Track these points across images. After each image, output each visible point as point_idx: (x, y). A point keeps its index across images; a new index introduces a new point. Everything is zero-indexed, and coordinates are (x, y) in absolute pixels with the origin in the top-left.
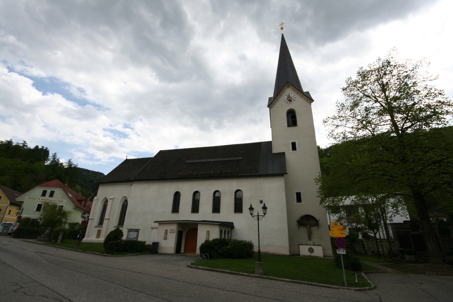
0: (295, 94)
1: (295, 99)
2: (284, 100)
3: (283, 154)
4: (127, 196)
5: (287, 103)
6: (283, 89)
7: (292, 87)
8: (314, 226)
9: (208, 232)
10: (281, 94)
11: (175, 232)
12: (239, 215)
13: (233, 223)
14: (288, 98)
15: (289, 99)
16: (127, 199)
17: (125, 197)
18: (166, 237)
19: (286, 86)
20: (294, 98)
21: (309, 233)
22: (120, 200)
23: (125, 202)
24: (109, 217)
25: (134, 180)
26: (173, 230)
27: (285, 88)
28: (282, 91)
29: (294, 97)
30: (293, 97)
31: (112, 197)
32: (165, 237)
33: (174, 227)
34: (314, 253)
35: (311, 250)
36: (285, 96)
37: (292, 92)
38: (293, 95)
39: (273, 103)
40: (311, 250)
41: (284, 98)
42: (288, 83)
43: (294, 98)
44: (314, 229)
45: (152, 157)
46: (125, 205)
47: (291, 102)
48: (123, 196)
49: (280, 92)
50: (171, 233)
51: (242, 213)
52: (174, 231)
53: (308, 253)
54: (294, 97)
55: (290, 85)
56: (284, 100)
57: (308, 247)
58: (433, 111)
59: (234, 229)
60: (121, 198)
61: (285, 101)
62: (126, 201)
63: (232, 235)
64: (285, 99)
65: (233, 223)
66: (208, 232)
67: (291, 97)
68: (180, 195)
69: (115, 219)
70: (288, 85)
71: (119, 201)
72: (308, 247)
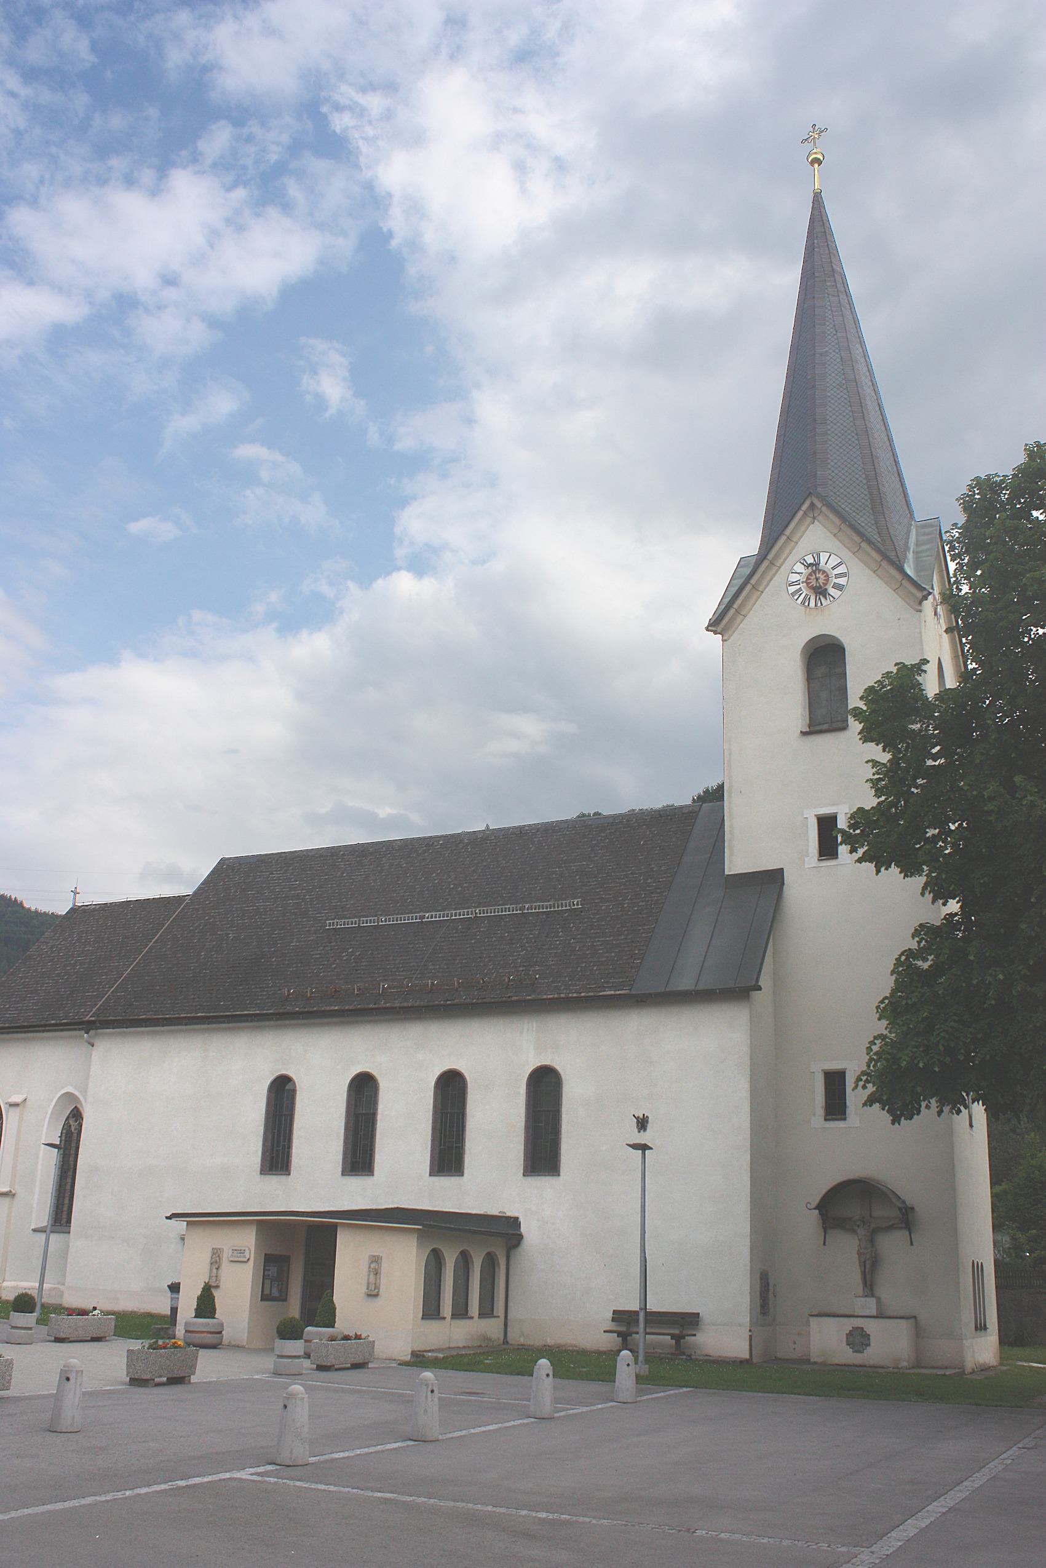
0: (847, 555)
1: (842, 581)
2: (792, 589)
3: (773, 879)
4: (77, 1094)
5: (803, 603)
6: (788, 532)
7: (831, 516)
8: (890, 1228)
9: (376, 1260)
10: (777, 556)
11: (249, 1259)
12: (544, 1184)
13: (517, 1219)
14: (810, 574)
15: (814, 583)
16: (78, 1106)
17: (69, 1096)
18: (377, 1287)
19: (800, 514)
20: (837, 576)
21: (865, 1262)
22: (52, 1113)
23: (71, 1122)
24: (12, 1184)
25: (100, 1021)
26: (242, 1252)
27: (800, 520)
28: (783, 539)
29: (841, 569)
30: (833, 568)
31: (17, 1099)
32: (214, 1279)
33: (247, 1240)
34: (869, 1351)
35: (858, 1339)
36: (799, 568)
37: (833, 544)
38: (834, 561)
39: (736, 606)
40: (858, 1339)
41: (794, 578)
42: (810, 494)
43: (837, 576)
44: (892, 1244)
45: (178, 900)
46: (72, 1133)
47: (823, 600)
48: (59, 1095)
49: (787, 526)
50: (233, 1264)
51: (559, 1175)
52: (247, 1255)
53: (845, 1355)
54: (841, 569)
55: (819, 504)
56: (792, 589)
57: (848, 1324)
58: (923, 867)
59: (520, 1249)
60: (53, 1104)
61: (793, 594)
62: (76, 1115)
63: (511, 1273)
64: (797, 583)
65: (517, 1219)
66: (376, 1260)
67: (824, 572)
68: (293, 1093)
69: (36, 1196)
70: (812, 505)
71: (48, 1116)
72: (848, 1324)
